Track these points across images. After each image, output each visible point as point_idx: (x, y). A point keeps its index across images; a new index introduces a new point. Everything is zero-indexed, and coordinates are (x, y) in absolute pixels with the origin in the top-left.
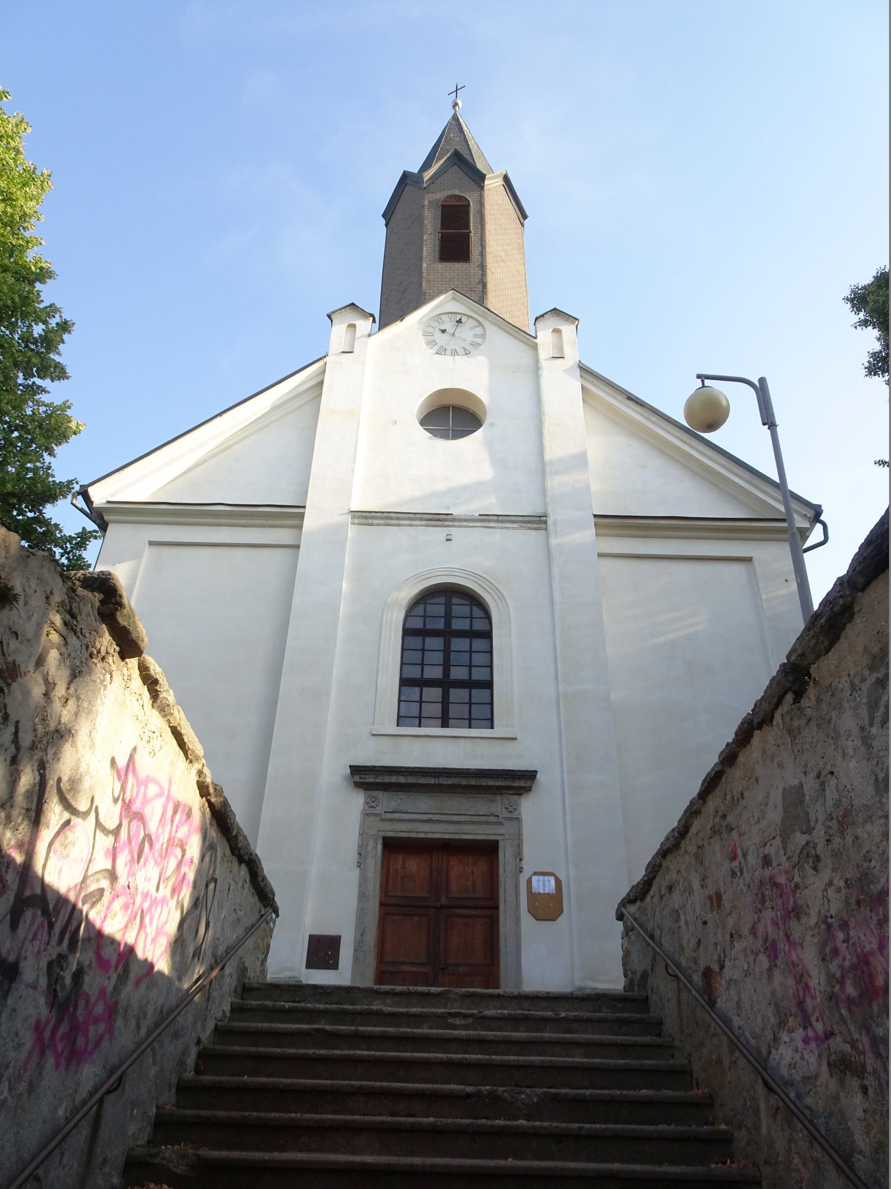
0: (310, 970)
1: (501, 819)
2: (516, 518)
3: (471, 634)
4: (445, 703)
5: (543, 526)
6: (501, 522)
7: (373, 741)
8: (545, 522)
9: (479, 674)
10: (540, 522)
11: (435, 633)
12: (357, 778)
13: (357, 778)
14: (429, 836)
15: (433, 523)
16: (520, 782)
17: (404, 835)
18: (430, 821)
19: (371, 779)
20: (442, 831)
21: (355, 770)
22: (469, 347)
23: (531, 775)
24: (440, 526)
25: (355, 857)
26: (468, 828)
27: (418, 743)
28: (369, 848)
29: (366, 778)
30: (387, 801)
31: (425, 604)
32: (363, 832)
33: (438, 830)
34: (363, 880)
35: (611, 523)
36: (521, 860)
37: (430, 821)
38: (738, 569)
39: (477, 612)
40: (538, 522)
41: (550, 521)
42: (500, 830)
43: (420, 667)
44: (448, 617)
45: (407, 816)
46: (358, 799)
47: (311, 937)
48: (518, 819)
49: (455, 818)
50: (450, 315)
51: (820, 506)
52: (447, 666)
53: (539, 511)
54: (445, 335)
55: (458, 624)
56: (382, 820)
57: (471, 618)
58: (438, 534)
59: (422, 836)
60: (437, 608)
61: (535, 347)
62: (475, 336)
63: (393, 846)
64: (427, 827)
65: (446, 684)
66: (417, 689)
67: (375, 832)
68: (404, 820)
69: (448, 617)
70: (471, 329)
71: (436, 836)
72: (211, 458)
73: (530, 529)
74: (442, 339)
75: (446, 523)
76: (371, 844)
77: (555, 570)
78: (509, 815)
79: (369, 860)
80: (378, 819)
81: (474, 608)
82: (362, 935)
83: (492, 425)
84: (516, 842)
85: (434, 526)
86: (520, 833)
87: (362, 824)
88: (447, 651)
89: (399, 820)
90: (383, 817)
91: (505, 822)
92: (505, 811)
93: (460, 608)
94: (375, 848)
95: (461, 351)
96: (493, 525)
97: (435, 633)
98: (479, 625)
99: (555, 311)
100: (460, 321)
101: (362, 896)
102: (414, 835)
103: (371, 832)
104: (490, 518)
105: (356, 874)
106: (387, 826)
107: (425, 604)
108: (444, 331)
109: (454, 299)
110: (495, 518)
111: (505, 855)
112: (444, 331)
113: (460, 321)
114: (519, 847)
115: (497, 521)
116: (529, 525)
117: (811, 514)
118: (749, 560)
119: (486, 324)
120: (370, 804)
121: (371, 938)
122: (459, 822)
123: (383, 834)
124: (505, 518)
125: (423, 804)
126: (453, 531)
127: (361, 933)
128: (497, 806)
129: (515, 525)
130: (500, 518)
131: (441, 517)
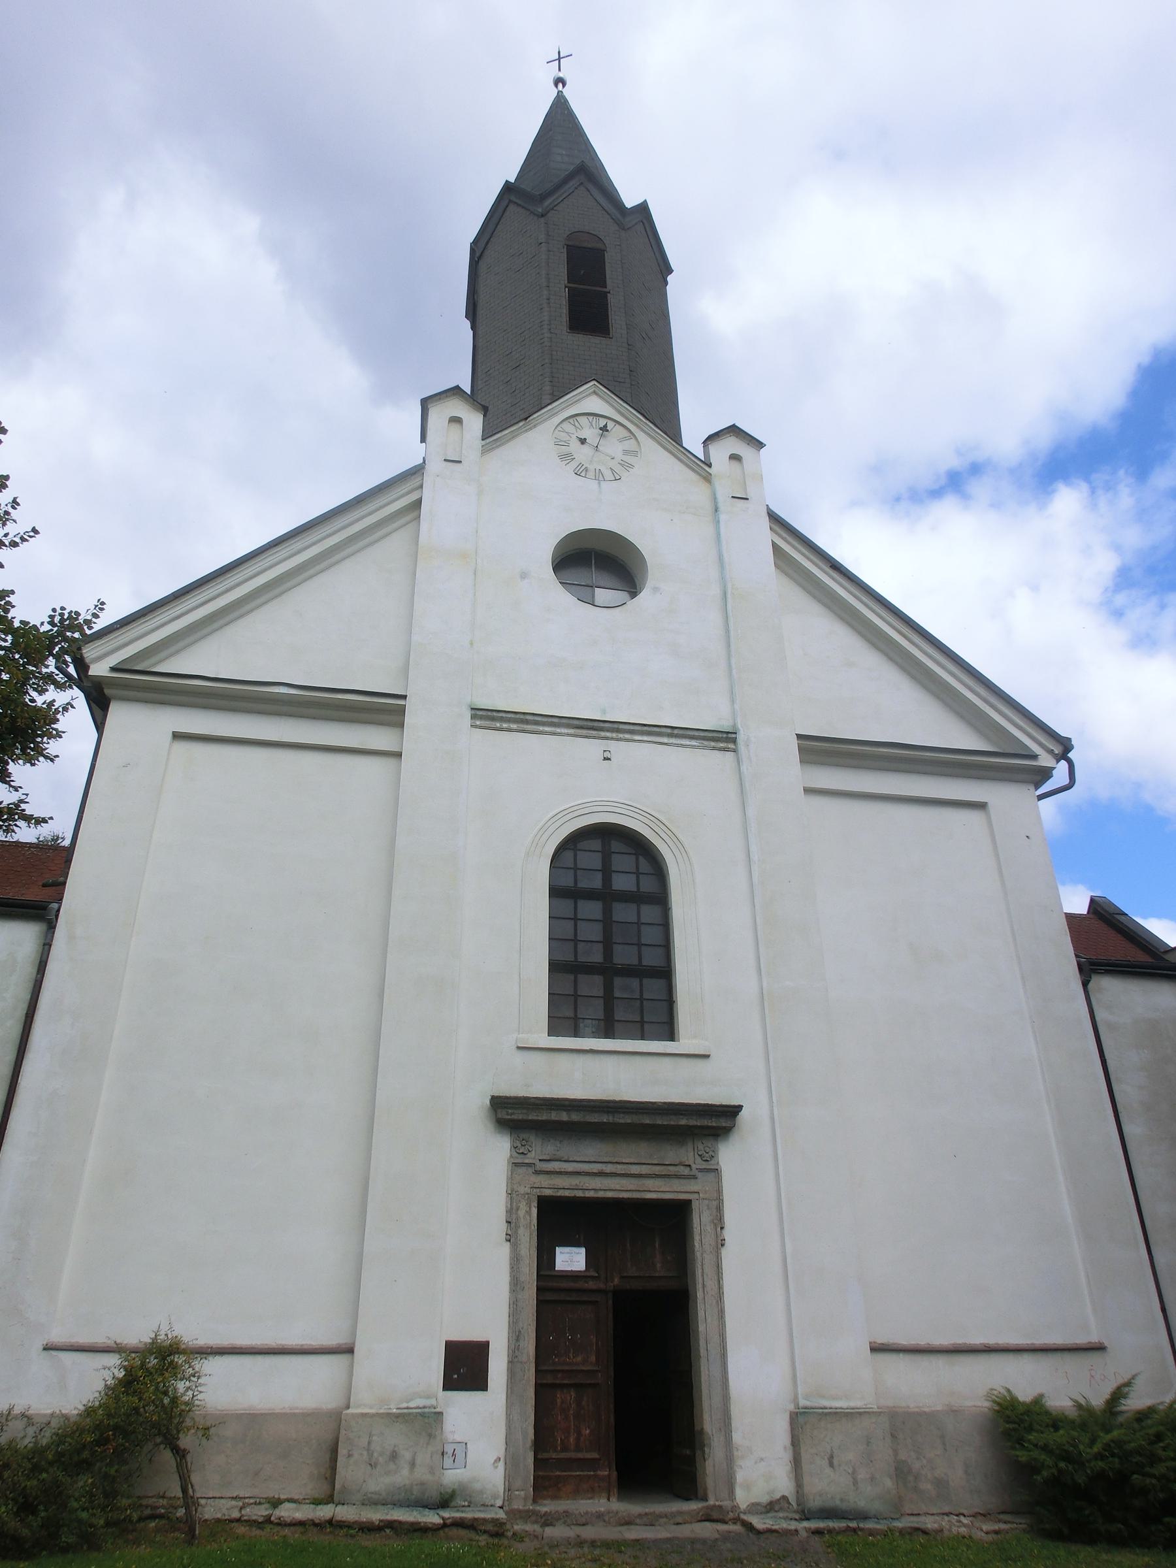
0: (449, 1393)
1: (694, 1172)
2: (696, 733)
3: (635, 898)
4: (609, 1000)
5: (731, 746)
6: (677, 736)
7: (520, 1058)
8: (734, 741)
9: (651, 959)
10: (728, 740)
11: (590, 895)
12: (503, 1114)
13: (503, 1114)
14: (601, 1194)
15: (584, 732)
16: (717, 1121)
17: (567, 1193)
18: (601, 1174)
19: (519, 1115)
20: (618, 1187)
21: (799, 736)
22: (618, 469)
23: (733, 1112)
24: (594, 738)
25: (504, 1226)
26: (650, 1183)
27: (580, 1060)
28: (521, 1213)
29: (516, 1116)
30: (540, 1149)
31: (575, 850)
32: (512, 1190)
33: (613, 1187)
34: (515, 1261)
35: (818, 750)
36: (722, 1228)
37: (601, 1174)
38: (973, 818)
39: (645, 866)
40: (724, 739)
41: (741, 738)
42: (693, 1186)
43: (572, 943)
44: (607, 872)
45: (570, 1167)
46: (501, 1147)
47: (487, 1343)
48: (716, 1171)
49: (635, 1169)
50: (591, 418)
51: (1070, 739)
52: (607, 944)
53: (724, 725)
54: (585, 447)
55: (622, 883)
56: (537, 1173)
57: (638, 874)
58: (592, 748)
59: (591, 1194)
60: (591, 859)
61: (708, 478)
62: (626, 452)
63: (557, 1219)
64: (597, 1183)
65: (608, 971)
66: (600, 938)
67: (528, 1190)
68: (567, 1173)
69: (607, 872)
70: (620, 440)
71: (610, 1195)
72: (763, 1008)
73: (714, 748)
74: (583, 454)
75: (603, 734)
76: (523, 1206)
77: (751, 812)
78: (704, 1165)
79: (521, 1231)
80: (531, 1170)
81: (641, 859)
82: (517, 1340)
83: (656, 589)
84: (715, 1203)
85: (586, 737)
86: (719, 1192)
87: (511, 1179)
88: (607, 922)
89: (560, 1173)
90: (538, 1168)
91: (699, 1175)
92: (699, 1160)
93: (623, 861)
94: (529, 1213)
95: (608, 474)
96: (665, 740)
97: (590, 895)
98: (648, 885)
99: (733, 430)
100: (604, 429)
101: (516, 1284)
102: (580, 1194)
103: (522, 1190)
104: (663, 730)
105: (506, 1249)
106: (544, 1181)
107: (575, 850)
108: (583, 441)
109: (594, 392)
110: (669, 731)
111: (700, 1221)
112: (583, 441)
113: (604, 429)
114: (719, 1209)
115: (670, 735)
116: (713, 744)
117: (1057, 750)
118: (981, 806)
119: (641, 436)
120: (518, 1150)
121: (529, 1346)
122: (640, 1176)
123: (538, 1192)
124: (681, 732)
125: (590, 1152)
126: (612, 745)
127: (515, 1336)
128: (687, 1154)
129: (694, 743)
130: (676, 731)
131: (596, 724)
